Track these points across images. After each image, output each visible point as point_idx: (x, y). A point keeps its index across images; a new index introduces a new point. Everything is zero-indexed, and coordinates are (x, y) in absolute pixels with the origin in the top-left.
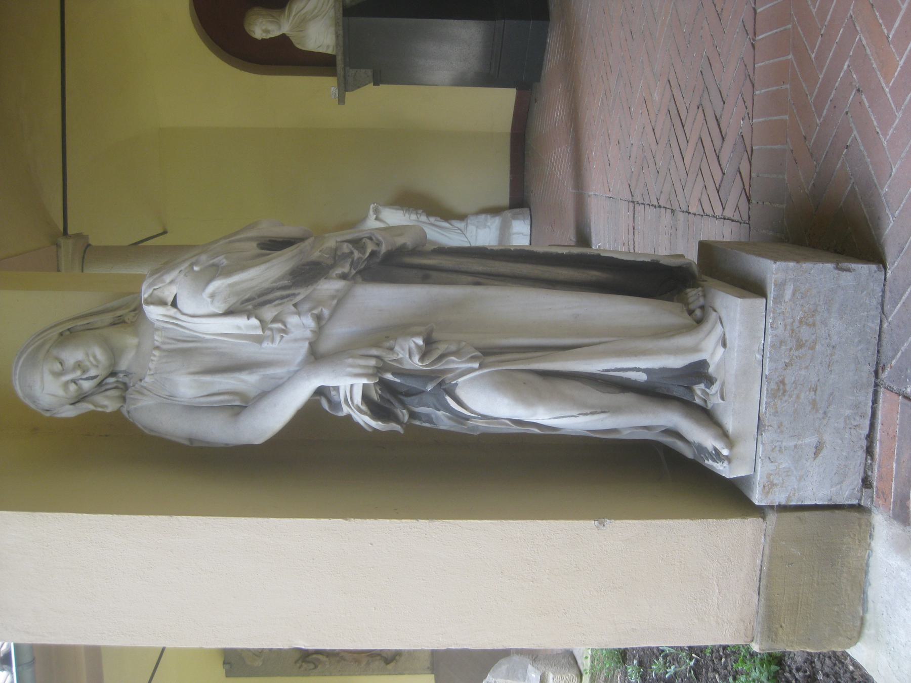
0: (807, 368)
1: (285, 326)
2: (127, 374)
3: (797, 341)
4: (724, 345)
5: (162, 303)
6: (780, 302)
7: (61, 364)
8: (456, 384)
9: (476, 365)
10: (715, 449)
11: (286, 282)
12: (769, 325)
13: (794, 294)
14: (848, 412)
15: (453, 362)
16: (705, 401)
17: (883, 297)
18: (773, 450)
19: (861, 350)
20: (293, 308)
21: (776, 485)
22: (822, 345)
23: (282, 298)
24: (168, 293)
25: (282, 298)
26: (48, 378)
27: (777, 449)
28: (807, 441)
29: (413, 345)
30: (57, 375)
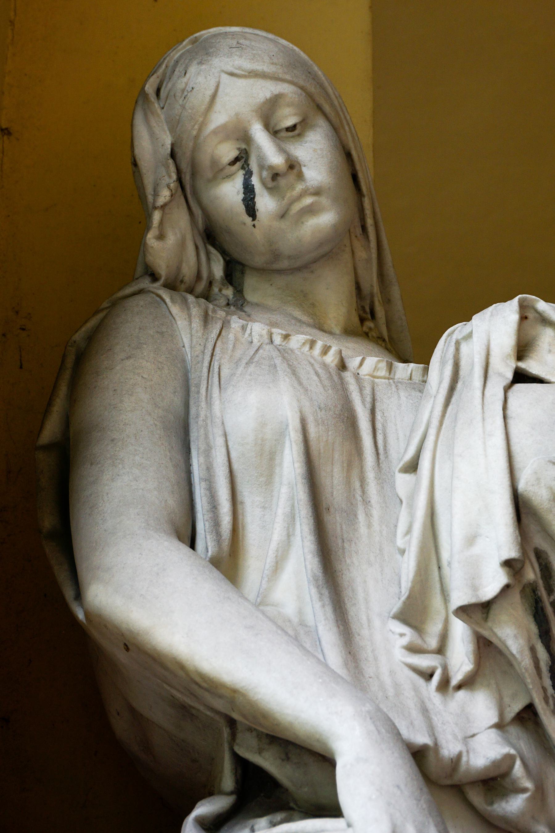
1: (459, 687)
5: (523, 350)
7: (292, 128)
20: (517, 707)
26: (265, 90)
30: (267, 114)
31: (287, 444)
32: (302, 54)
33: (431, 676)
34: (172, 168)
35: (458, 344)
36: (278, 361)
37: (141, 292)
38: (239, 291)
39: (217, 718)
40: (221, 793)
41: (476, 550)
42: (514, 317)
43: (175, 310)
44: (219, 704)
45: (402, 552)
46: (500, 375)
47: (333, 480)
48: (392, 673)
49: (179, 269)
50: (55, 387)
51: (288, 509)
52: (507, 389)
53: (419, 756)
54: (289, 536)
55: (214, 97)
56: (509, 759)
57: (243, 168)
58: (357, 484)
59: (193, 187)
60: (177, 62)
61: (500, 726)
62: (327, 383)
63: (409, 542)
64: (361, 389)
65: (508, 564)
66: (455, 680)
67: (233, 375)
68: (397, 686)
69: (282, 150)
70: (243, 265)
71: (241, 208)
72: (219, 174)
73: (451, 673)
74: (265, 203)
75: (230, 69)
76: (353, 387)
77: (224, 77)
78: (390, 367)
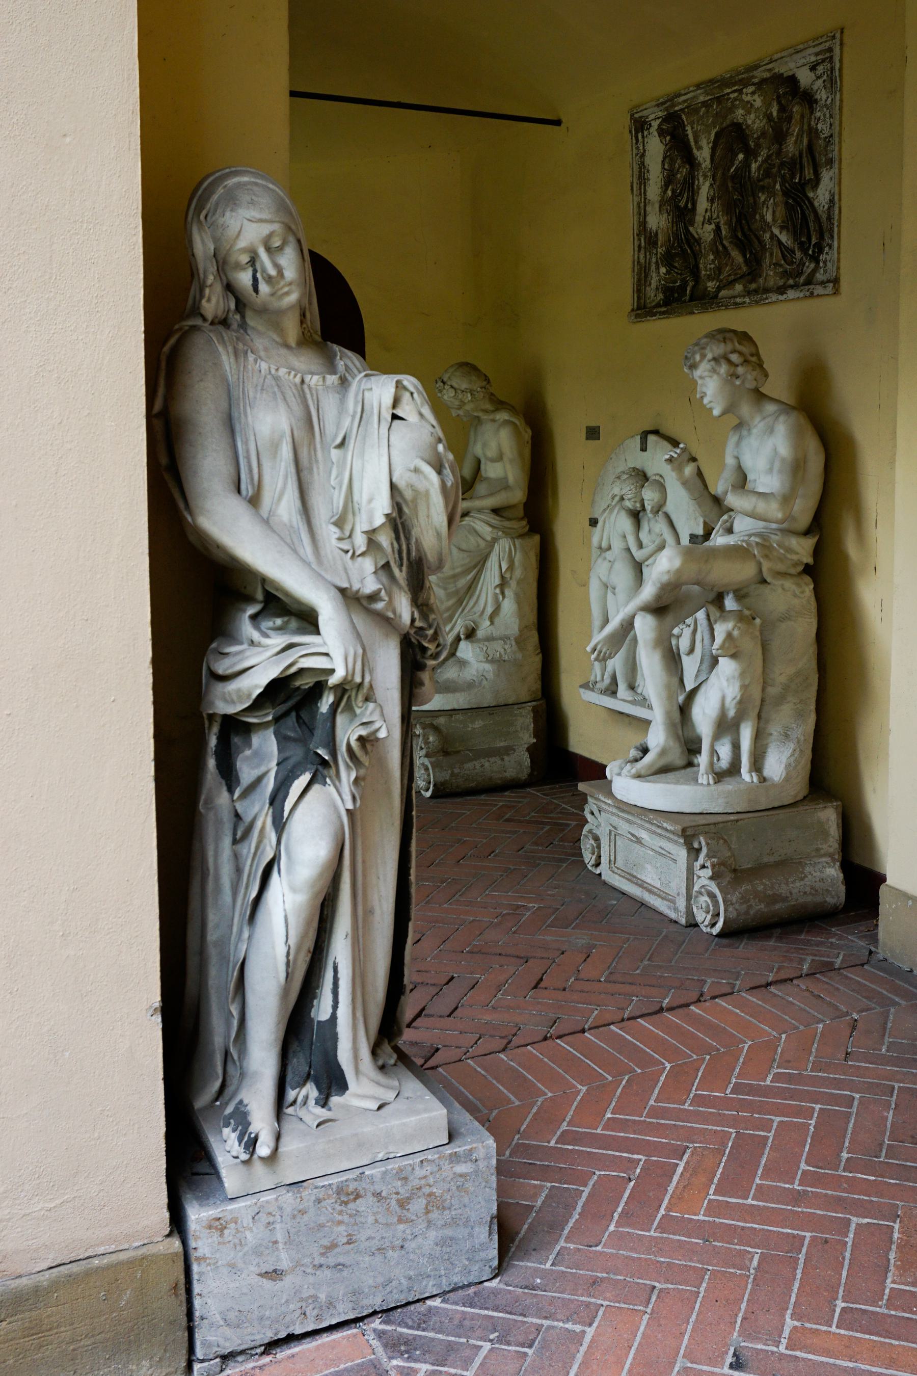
0: (376, 1221)
1: (359, 556)
2: (243, 325)
3: (408, 1198)
4: (379, 1108)
5: (396, 403)
6: (451, 1162)
8: (325, 784)
9: (350, 806)
10: (256, 1139)
11: (414, 554)
13: (461, 1175)
14: (322, 1297)
15: (349, 776)
17: (464, 1287)
18: (270, 1213)
19: (400, 1284)
20: (382, 563)
21: (222, 1235)
22: (404, 1232)
24: (406, 409)
25: (400, 552)
26: (266, 229)
27: (271, 1219)
28: (284, 1255)
29: (377, 725)
34: (215, 263)
41: (372, 505)
53: (343, 591)
54: (285, 484)
55: (240, 232)
64: (312, 395)
65: (387, 515)
71: (251, 288)
72: (239, 267)
74: (264, 288)
77: (245, 222)
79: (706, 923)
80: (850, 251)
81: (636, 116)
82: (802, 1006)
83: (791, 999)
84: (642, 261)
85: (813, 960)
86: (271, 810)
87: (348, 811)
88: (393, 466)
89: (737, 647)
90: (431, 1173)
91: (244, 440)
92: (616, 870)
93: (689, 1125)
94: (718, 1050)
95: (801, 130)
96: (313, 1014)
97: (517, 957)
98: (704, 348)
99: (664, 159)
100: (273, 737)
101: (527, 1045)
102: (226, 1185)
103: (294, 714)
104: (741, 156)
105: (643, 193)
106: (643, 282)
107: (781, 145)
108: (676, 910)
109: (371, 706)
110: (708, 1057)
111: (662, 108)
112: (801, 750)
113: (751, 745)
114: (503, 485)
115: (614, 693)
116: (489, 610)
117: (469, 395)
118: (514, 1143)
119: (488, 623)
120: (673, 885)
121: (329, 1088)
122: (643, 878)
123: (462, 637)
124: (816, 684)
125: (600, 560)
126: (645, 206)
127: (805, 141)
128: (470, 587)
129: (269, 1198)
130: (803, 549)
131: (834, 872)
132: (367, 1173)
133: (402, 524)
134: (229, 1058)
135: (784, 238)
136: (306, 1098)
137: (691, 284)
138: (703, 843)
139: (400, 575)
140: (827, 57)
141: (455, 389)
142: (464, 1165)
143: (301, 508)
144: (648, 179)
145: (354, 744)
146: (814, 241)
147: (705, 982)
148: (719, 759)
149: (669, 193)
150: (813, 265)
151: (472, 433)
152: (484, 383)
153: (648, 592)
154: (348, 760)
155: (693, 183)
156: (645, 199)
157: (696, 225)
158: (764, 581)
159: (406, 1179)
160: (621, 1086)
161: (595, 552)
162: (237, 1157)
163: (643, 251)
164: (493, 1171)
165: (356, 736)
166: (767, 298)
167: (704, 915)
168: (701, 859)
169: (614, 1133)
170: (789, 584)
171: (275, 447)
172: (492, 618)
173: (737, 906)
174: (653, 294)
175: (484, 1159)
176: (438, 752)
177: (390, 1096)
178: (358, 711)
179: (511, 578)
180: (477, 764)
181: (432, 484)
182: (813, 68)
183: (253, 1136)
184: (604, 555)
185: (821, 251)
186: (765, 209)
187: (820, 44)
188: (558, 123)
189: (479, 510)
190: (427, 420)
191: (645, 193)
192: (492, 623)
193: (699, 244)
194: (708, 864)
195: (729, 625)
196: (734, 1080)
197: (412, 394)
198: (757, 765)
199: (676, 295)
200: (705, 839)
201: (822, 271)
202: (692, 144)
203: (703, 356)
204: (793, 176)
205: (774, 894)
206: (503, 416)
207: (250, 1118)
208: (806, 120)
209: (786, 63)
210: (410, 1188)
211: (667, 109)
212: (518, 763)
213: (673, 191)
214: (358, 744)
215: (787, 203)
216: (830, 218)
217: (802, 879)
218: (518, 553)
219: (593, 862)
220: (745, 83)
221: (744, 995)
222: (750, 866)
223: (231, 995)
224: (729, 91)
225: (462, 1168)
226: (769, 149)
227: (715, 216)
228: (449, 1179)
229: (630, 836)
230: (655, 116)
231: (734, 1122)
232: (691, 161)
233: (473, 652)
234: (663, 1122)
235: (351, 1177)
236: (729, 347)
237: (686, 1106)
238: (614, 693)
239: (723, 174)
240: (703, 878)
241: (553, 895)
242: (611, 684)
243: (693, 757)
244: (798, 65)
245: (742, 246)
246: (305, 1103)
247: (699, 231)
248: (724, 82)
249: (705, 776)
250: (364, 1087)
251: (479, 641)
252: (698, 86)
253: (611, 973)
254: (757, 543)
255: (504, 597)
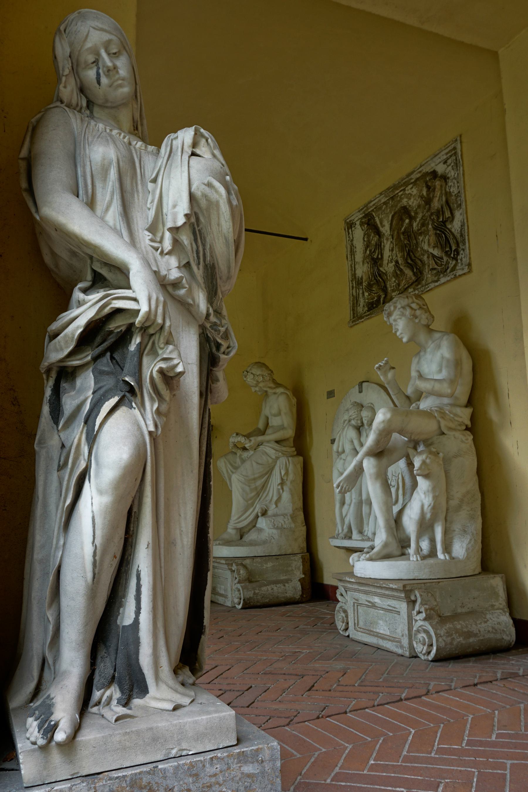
4: (175, 709)
5: (195, 144)
7: (115, 54)
8: (131, 407)
9: (152, 428)
10: (56, 725)
11: (208, 258)
12: (212, 755)
13: (249, 776)
16: (98, 703)
20: (184, 262)
23: (198, 252)
24: (203, 150)
25: (198, 252)
26: (106, 37)
29: (176, 362)
30: (107, 45)
31: (112, 167)
32: (119, 26)
33: (158, 250)
34: (70, 62)
35: (172, 140)
36: (109, 138)
37: (57, 107)
38: (92, 112)
39: (86, 256)
40: (86, 281)
41: (176, 210)
42: (193, 133)
43: (71, 115)
44: (89, 252)
45: (149, 209)
46: (187, 152)
47: (127, 182)
48: (145, 247)
49: (71, 100)
50: (25, 138)
51: (112, 190)
52: (189, 157)
53: (156, 273)
55: (87, 36)
56: (182, 278)
57: (96, 66)
58: (135, 185)
59: (77, 70)
60: (73, 20)
61: (178, 267)
62: (125, 148)
63: (153, 206)
64: (136, 153)
65: (186, 215)
66: (165, 252)
67: (93, 141)
68: (147, 252)
69: (111, 61)
70: (93, 103)
71: (95, 81)
72: (87, 66)
73: (164, 249)
74: (104, 80)
75: (93, 26)
76: (134, 151)
77: (91, 29)
78: (146, 147)
79: (424, 652)
80: (475, 249)
81: (348, 221)
82: (505, 695)
83: (494, 692)
84: (354, 294)
85: (502, 672)
86: (85, 429)
87: (150, 433)
88: (192, 181)
89: (429, 470)
90: (221, 772)
91: (82, 165)
92: (359, 629)
93: (439, 767)
94: (449, 721)
95: (441, 193)
96: (118, 622)
97: (296, 675)
98: (395, 303)
99: (364, 236)
100: (91, 374)
101: (305, 721)
102: (23, 772)
103: (108, 354)
104: (407, 221)
105: (353, 259)
106: (355, 305)
107: (430, 205)
108: (402, 647)
109: (171, 347)
110: (442, 725)
111: (361, 212)
112: (475, 540)
113: (442, 537)
114: (282, 428)
115: (350, 538)
116: (275, 498)
117: (261, 377)
118: (297, 782)
119: (274, 506)
120: (399, 631)
121: (131, 690)
122: (378, 631)
123: (259, 514)
124: (480, 500)
125: (338, 460)
126: (355, 266)
127: (444, 199)
128: (263, 486)
129: (64, 786)
130: (465, 415)
131: (506, 619)
132: (160, 767)
133: (199, 231)
134: (46, 664)
135: (436, 252)
136: (110, 698)
137: (383, 296)
138: (418, 595)
139: (199, 272)
140: (454, 152)
141: (254, 375)
142: (251, 765)
143: (123, 213)
144: (356, 252)
145: (155, 374)
146: (454, 248)
147: (429, 684)
148: (422, 550)
149: (368, 252)
150: (454, 262)
151: (264, 404)
152: (270, 372)
153: (370, 439)
154: (151, 391)
155: (381, 245)
156: (354, 262)
157: (384, 266)
158: (443, 433)
159: (197, 775)
160: (379, 744)
161: (335, 455)
162: (34, 743)
163: (354, 289)
164: (278, 773)
165: (156, 368)
166: (428, 287)
167: (422, 647)
168: (417, 608)
169: (378, 774)
170: (458, 434)
171: (105, 171)
172: (276, 504)
173: (444, 638)
174: (360, 309)
175: (270, 761)
176: (245, 580)
177: (186, 701)
178: (160, 352)
179: (287, 480)
180: (269, 588)
181: (221, 195)
182: (445, 162)
183: (53, 723)
184: (340, 456)
185: (458, 254)
186: (423, 244)
187: (448, 147)
188: (306, 239)
189: (268, 442)
190: (218, 160)
191: (354, 259)
192: (277, 506)
193: (386, 275)
194: (422, 610)
195: (424, 456)
196: (466, 738)
197: (207, 141)
198: (447, 549)
199: (375, 306)
200: (419, 592)
201: (460, 264)
202: (379, 225)
203: (395, 307)
204: (438, 218)
205: (468, 632)
206: (280, 390)
207: (53, 710)
208: (443, 188)
209: (430, 164)
210: (201, 785)
211: (364, 212)
212: (293, 588)
213: (370, 251)
214: (160, 375)
215: (436, 234)
216: (462, 235)
217: (486, 622)
218: (291, 464)
219: (343, 627)
220: (406, 184)
221: (460, 690)
222: (449, 614)
223: (47, 600)
224: (398, 191)
225: (249, 769)
226: (423, 213)
227: (394, 257)
228: (238, 778)
229: (367, 603)
230: (357, 217)
231: (475, 764)
232: (378, 233)
233: (266, 523)
234: (416, 765)
235: (145, 770)
236: (410, 300)
237: (433, 755)
238: (350, 538)
239: (398, 233)
240: (419, 621)
241: (319, 646)
242: (348, 532)
243: (405, 550)
244: (436, 163)
245: (411, 267)
246: (109, 702)
247: (386, 268)
248: (395, 187)
249: (414, 556)
250: (161, 695)
251: (269, 517)
252: (381, 194)
253: (362, 682)
254: (436, 410)
255: (283, 491)
